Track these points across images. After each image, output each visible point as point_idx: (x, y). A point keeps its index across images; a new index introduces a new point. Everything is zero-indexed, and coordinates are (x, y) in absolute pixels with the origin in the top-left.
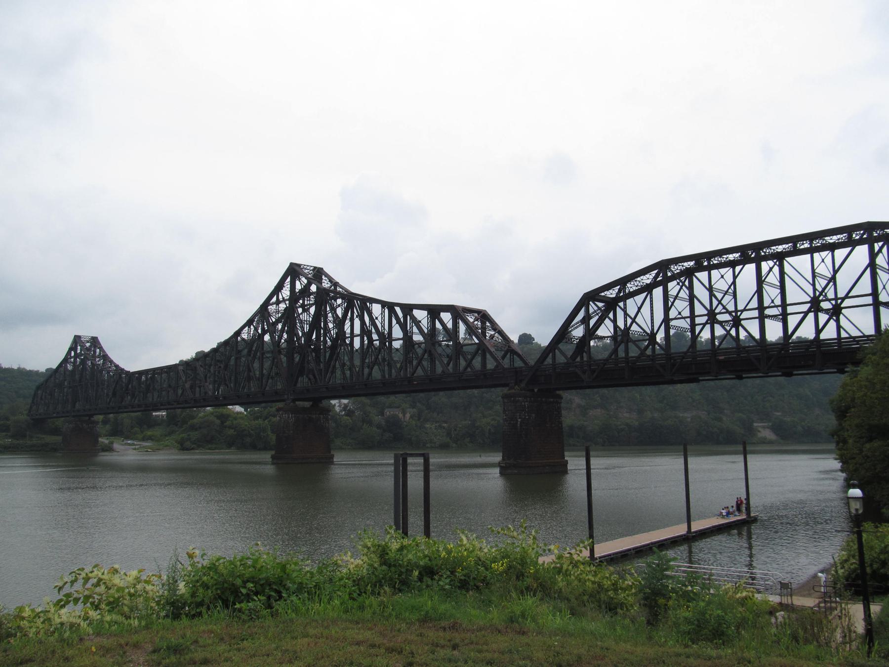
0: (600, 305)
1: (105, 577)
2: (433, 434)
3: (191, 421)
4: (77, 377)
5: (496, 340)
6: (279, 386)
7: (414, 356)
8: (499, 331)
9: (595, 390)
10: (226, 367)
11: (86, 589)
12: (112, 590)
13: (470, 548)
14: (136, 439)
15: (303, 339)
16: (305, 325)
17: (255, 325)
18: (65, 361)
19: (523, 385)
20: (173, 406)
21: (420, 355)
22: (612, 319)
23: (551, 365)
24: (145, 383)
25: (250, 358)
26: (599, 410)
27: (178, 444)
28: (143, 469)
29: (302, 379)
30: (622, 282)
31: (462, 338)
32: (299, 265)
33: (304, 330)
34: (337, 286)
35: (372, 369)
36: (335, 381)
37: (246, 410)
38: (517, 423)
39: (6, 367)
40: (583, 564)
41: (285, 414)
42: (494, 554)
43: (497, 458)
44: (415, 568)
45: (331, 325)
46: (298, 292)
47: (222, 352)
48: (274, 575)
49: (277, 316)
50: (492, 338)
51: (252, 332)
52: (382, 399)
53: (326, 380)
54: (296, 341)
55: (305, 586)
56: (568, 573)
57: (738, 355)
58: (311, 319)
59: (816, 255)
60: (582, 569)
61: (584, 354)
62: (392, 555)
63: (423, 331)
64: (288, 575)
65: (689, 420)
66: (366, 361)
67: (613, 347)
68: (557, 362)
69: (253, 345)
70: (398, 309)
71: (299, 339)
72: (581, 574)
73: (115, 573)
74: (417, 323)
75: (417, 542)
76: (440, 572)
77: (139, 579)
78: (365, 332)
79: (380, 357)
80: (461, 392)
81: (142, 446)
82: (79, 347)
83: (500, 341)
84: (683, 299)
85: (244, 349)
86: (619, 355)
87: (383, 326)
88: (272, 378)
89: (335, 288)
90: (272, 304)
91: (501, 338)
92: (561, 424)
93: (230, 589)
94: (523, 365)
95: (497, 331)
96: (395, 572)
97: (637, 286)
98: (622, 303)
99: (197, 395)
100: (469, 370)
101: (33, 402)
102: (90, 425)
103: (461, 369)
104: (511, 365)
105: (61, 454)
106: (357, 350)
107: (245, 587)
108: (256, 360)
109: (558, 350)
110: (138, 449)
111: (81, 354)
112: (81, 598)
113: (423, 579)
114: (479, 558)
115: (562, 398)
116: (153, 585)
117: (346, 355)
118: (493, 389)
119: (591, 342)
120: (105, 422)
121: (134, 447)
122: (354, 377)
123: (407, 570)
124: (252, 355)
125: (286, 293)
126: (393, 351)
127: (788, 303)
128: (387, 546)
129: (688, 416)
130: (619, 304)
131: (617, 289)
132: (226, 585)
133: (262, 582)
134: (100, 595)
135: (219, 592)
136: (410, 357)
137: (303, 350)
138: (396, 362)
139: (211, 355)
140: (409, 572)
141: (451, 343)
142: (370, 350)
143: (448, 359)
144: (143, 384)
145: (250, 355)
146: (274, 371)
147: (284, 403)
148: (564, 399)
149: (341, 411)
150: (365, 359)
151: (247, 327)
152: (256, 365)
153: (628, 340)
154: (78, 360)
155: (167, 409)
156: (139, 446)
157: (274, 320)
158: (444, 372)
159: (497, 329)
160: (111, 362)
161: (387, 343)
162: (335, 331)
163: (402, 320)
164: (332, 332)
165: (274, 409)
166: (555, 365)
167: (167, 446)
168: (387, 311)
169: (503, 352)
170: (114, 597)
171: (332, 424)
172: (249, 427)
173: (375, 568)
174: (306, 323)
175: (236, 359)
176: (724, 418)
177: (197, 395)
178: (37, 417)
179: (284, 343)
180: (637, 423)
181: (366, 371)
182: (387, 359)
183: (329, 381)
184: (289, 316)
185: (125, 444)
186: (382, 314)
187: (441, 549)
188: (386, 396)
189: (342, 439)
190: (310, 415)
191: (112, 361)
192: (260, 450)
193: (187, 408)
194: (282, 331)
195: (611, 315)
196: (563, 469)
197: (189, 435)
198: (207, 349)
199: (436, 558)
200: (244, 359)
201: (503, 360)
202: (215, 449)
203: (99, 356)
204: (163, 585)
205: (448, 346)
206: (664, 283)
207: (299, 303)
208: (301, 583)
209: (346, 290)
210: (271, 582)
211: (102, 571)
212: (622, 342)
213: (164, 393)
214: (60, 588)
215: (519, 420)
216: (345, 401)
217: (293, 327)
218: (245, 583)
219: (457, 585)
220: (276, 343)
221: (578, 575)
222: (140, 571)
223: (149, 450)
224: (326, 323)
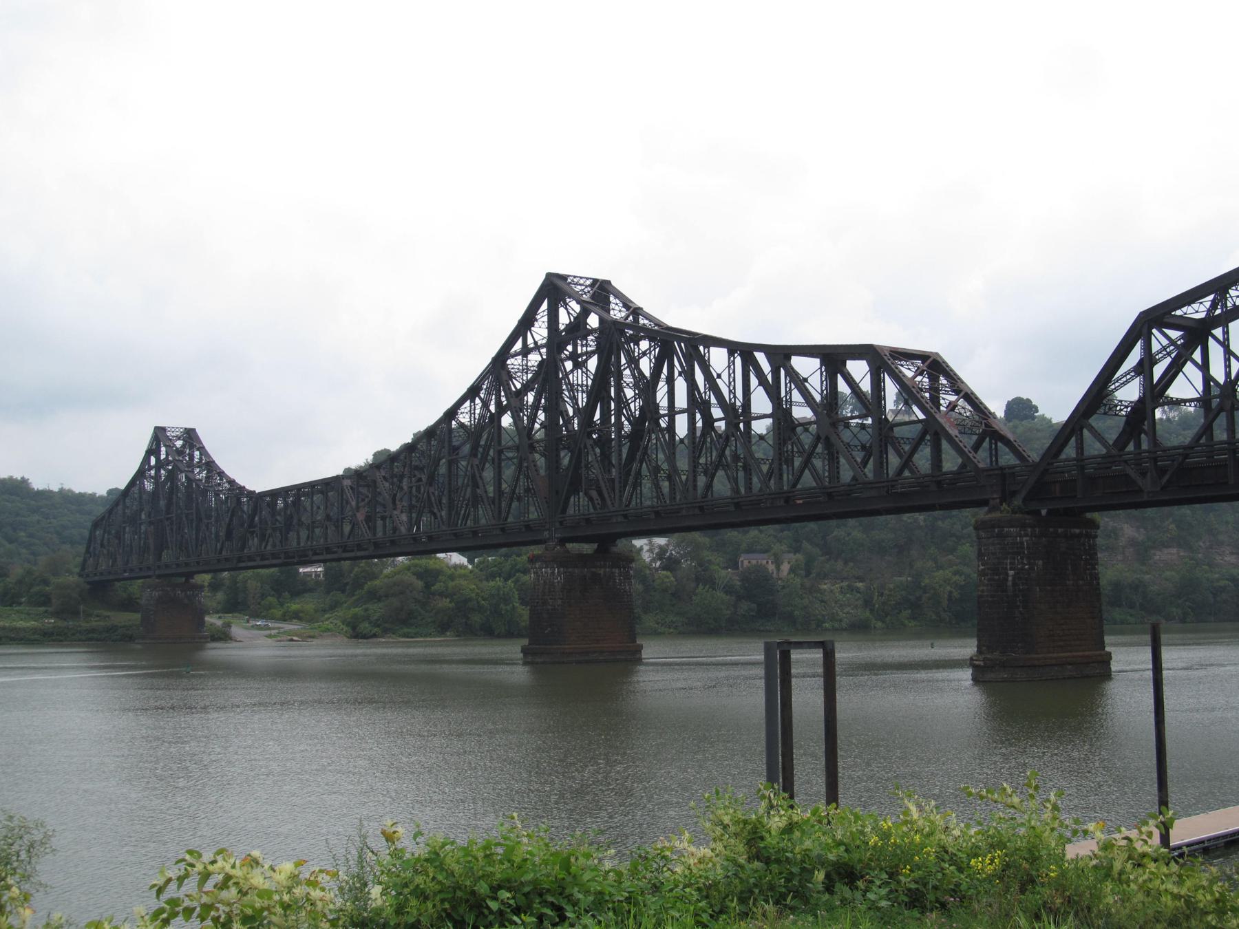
0: (1174, 334)
1: (237, 872)
2: (836, 602)
3: (369, 583)
4: (162, 503)
5: (960, 413)
6: (533, 515)
7: (795, 449)
8: (966, 393)
9: (1166, 509)
10: (432, 479)
11: (205, 893)
12: (249, 896)
13: (925, 828)
14: (273, 618)
15: (576, 421)
16: (580, 394)
17: (482, 396)
18: (141, 474)
19: (1017, 502)
21: (806, 447)
22: (1200, 363)
23: (1074, 459)
24: (283, 513)
25: (476, 461)
26: (1174, 551)
27: (347, 625)
28: (285, 673)
29: (576, 500)
31: (890, 410)
32: (564, 278)
33: (577, 403)
34: (638, 314)
35: (713, 476)
36: (641, 503)
37: (471, 561)
38: (1007, 580)
39: (40, 489)
40: (1156, 860)
41: (546, 567)
42: (973, 840)
43: (966, 648)
44: (819, 867)
45: (629, 393)
46: (564, 330)
47: (423, 452)
48: (548, 876)
49: (525, 378)
50: (953, 409)
51: (478, 411)
52: (732, 535)
53: (624, 499)
54: (562, 426)
55: (607, 898)
56: (1124, 877)
57: (1208, 457)
58: (590, 382)
60: (1153, 870)
61: (1143, 436)
62: (771, 840)
63: (813, 399)
64: (574, 877)
66: (701, 461)
67: (1202, 420)
68: (1086, 453)
69: (481, 437)
70: (761, 357)
71: (568, 421)
72: (1150, 880)
73: (254, 865)
74: (800, 382)
75: (820, 816)
76: (868, 874)
77: (296, 879)
78: (697, 404)
79: (727, 452)
80: (891, 518)
81: (282, 630)
82: (163, 449)
83: (968, 414)
85: (463, 444)
87: (732, 392)
88: (519, 499)
89: (636, 320)
91: (970, 408)
92: (1098, 579)
93: (467, 901)
94: (1018, 462)
95: (961, 395)
96: (780, 873)
98: (1220, 329)
99: (380, 534)
100: (907, 473)
101: (87, 551)
103: (891, 473)
104: (991, 461)
105: (139, 647)
106: (682, 441)
107: (495, 899)
108: (487, 465)
109: (1089, 430)
110: (275, 636)
111: (167, 462)
112: (195, 908)
113: (833, 887)
114: (943, 847)
115: (1098, 527)
116: (323, 889)
117: (660, 451)
118: (955, 512)
119: (1156, 410)
120: (214, 587)
121: (268, 632)
122: (677, 494)
123: (803, 869)
124: (479, 456)
125: (540, 332)
126: (754, 441)
128: (760, 823)
130: (1213, 332)
132: (459, 894)
133: (527, 889)
134: (229, 904)
135: (447, 905)
136: (787, 451)
137: (576, 443)
138: (758, 462)
139: (402, 457)
140: (807, 873)
141: (869, 421)
142: (709, 440)
143: (863, 453)
144: (279, 514)
145: (475, 456)
146: (521, 484)
147: (544, 546)
148: (1101, 528)
149: (654, 560)
150: (699, 457)
151: (469, 402)
152: (488, 474)
153: (1233, 405)
154: (162, 472)
155: (324, 561)
156: (277, 631)
157: (519, 386)
158: (857, 480)
159: (961, 391)
160: (221, 474)
161: (741, 425)
162: (637, 404)
163: (769, 378)
164: (632, 406)
165: (525, 558)
166: (1083, 460)
167: (328, 630)
168: (738, 361)
169: (975, 438)
170: (253, 907)
171: (637, 586)
173: (742, 867)
174: (580, 389)
175: (450, 463)
177: (380, 534)
178: (96, 578)
179: (539, 430)
181: (702, 480)
182: (742, 456)
183: (630, 503)
185: (253, 626)
186: (729, 367)
187: (868, 830)
188: (741, 529)
189: (657, 614)
190: (594, 570)
191: (223, 472)
192: (499, 636)
193: (362, 558)
194: (536, 406)
195: (1197, 355)
196: (1101, 670)
197: (366, 610)
198: (394, 446)
199: (858, 847)
200: (464, 463)
201: (976, 452)
202: (416, 635)
203: (199, 465)
204: (341, 889)
205: (863, 426)
207: (565, 352)
208: (601, 893)
209: (658, 323)
210: (544, 888)
211: (232, 861)
212: (1221, 409)
213: (317, 531)
214: (160, 891)
215: (1011, 573)
216: (661, 541)
217: (557, 398)
218: (495, 889)
219: (903, 901)
220: (525, 431)
221: (1145, 881)
222: (298, 864)
223: (295, 638)
224: (619, 389)
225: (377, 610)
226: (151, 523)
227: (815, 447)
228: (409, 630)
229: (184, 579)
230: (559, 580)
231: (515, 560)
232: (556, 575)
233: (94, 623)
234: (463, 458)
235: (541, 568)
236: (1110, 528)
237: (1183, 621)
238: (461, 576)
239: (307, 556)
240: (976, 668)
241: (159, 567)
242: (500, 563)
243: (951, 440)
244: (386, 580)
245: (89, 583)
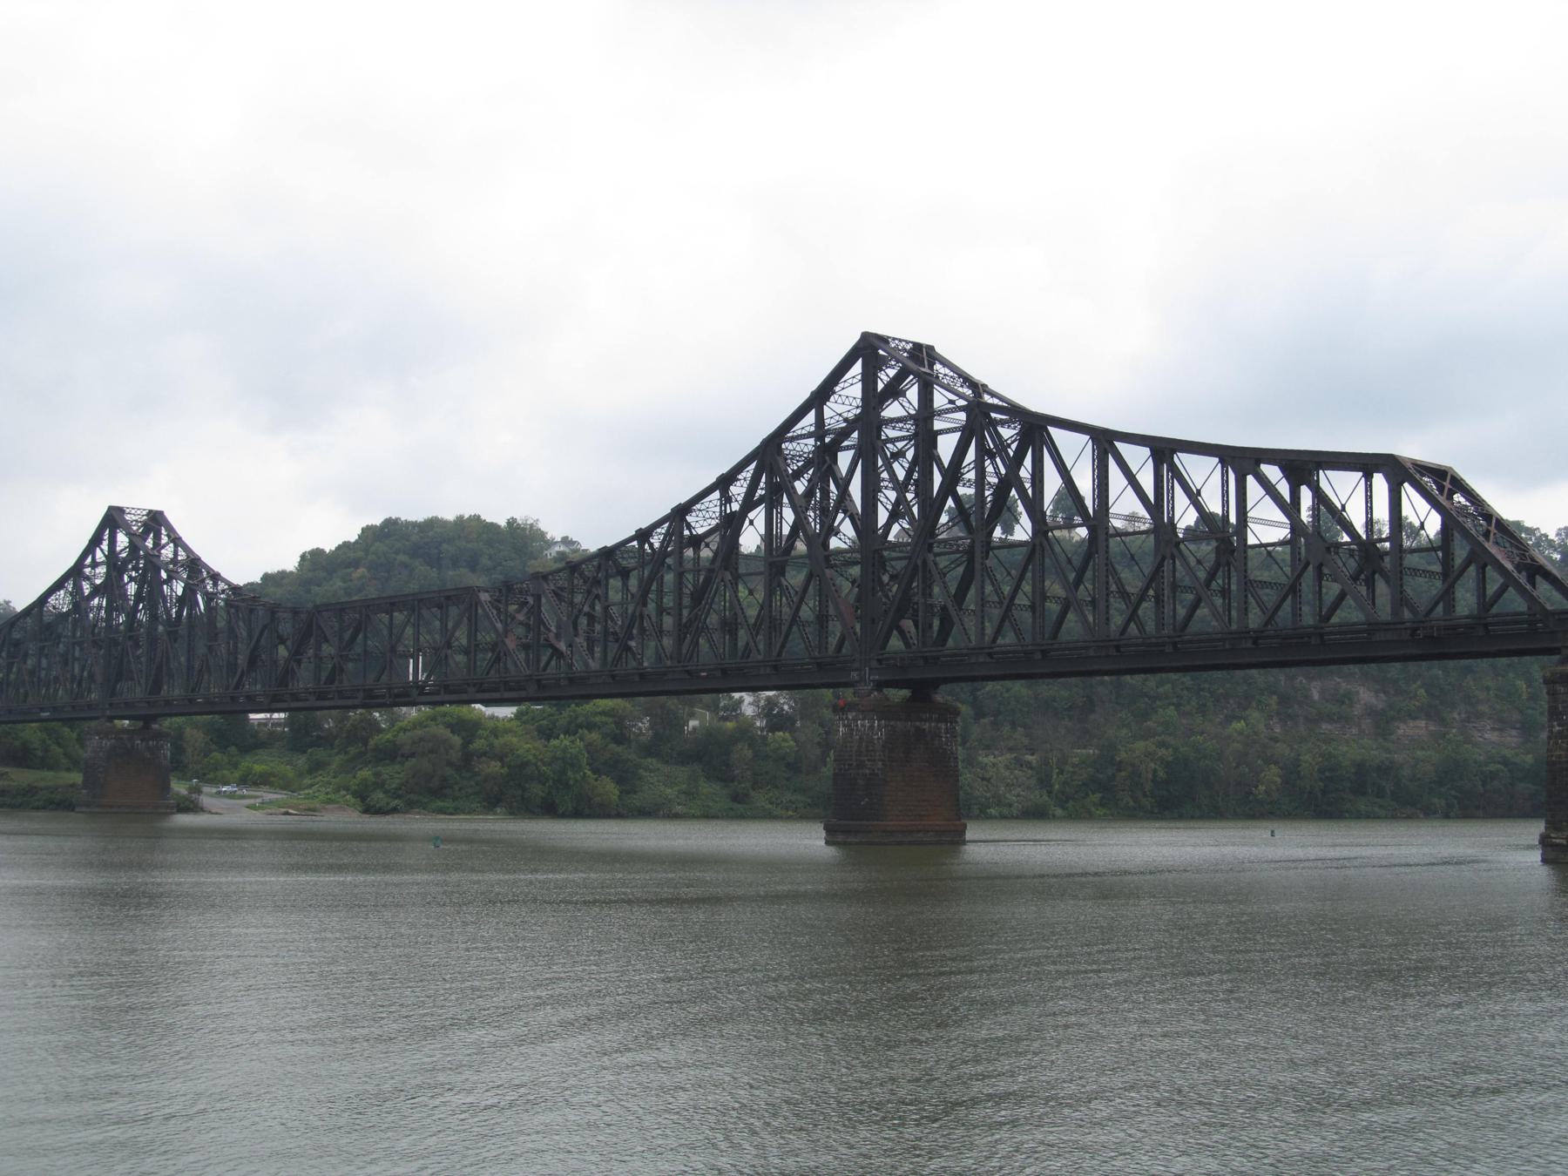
9: (1412, 667)
20: (307, 704)
26: (1422, 723)
41: (863, 719)
102: (151, 743)
190: (918, 724)
197: (377, 775)
202: (456, 811)
225: (394, 774)
228: (446, 804)
230: (880, 735)
231: (574, 711)
232: (874, 729)
235: (855, 720)
236: (1341, 691)
242: (551, 715)
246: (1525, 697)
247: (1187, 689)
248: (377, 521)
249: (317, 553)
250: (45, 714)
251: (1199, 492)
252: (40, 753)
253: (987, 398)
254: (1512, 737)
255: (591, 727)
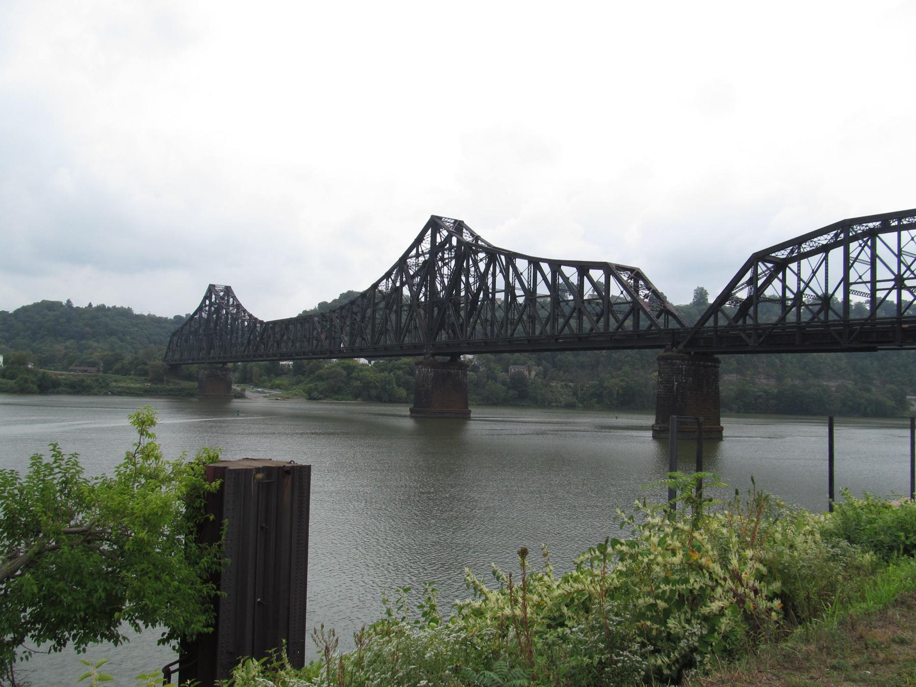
0: (770, 265)
14: (265, 387)
18: (200, 309)
20: (308, 357)
28: (270, 415)
30: (798, 241)
32: (440, 218)
37: (370, 362)
38: (673, 387)
45: (471, 280)
52: (506, 355)
59: (904, 234)
65: (833, 389)
71: (459, 291)
82: (213, 296)
84: (863, 262)
86: (640, 326)
89: (477, 242)
90: (411, 258)
97: (811, 247)
101: (168, 348)
106: (499, 306)
111: (216, 303)
121: (264, 395)
125: (426, 245)
127: (877, 279)
129: (833, 385)
131: (789, 250)
139: (347, 307)
147: (423, 357)
151: (385, 280)
160: (245, 311)
167: (296, 395)
172: (375, 380)
176: (874, 389)
178: (173, 363)
180: (776, 391)
184: (429, 270)
192: (385, 402)
193: (313, 359)
195: (780, 276)
202: (342, 399)
206: (846, 243)
209: (489, 245)
215: (676, 383)
225: (322, 385)
226: (205, 335)
227: (572, 313)
229: (222, 365)
232: (429, 372)
233: (171, 386)
234: (381, 309)
235: (422, 368)
237: (738, 412)
238: (366, 370)
239: (292, 356)
240: (654, 431)
241: (209, 358)
243: (645, 312)
244: (327, 370)
245: (169, 365)
246: (779, 366)
247: (638, 359)
248: (345, 291)
249: (325, 303)
250: (190, 361)
251: (522, 274)
252: (195, 376)
253: (480, 242)
254: (773, 382)
255: (399, 369)
